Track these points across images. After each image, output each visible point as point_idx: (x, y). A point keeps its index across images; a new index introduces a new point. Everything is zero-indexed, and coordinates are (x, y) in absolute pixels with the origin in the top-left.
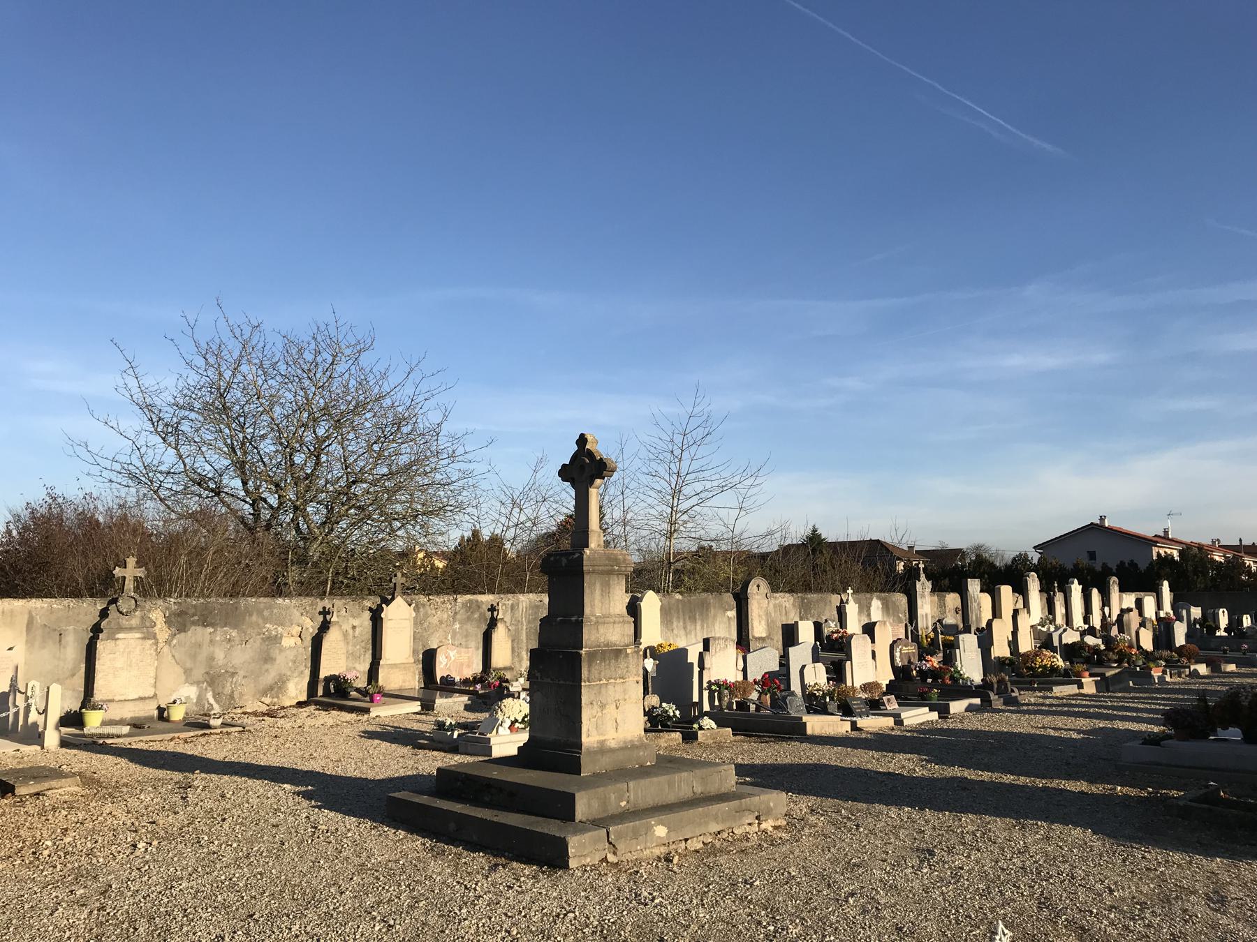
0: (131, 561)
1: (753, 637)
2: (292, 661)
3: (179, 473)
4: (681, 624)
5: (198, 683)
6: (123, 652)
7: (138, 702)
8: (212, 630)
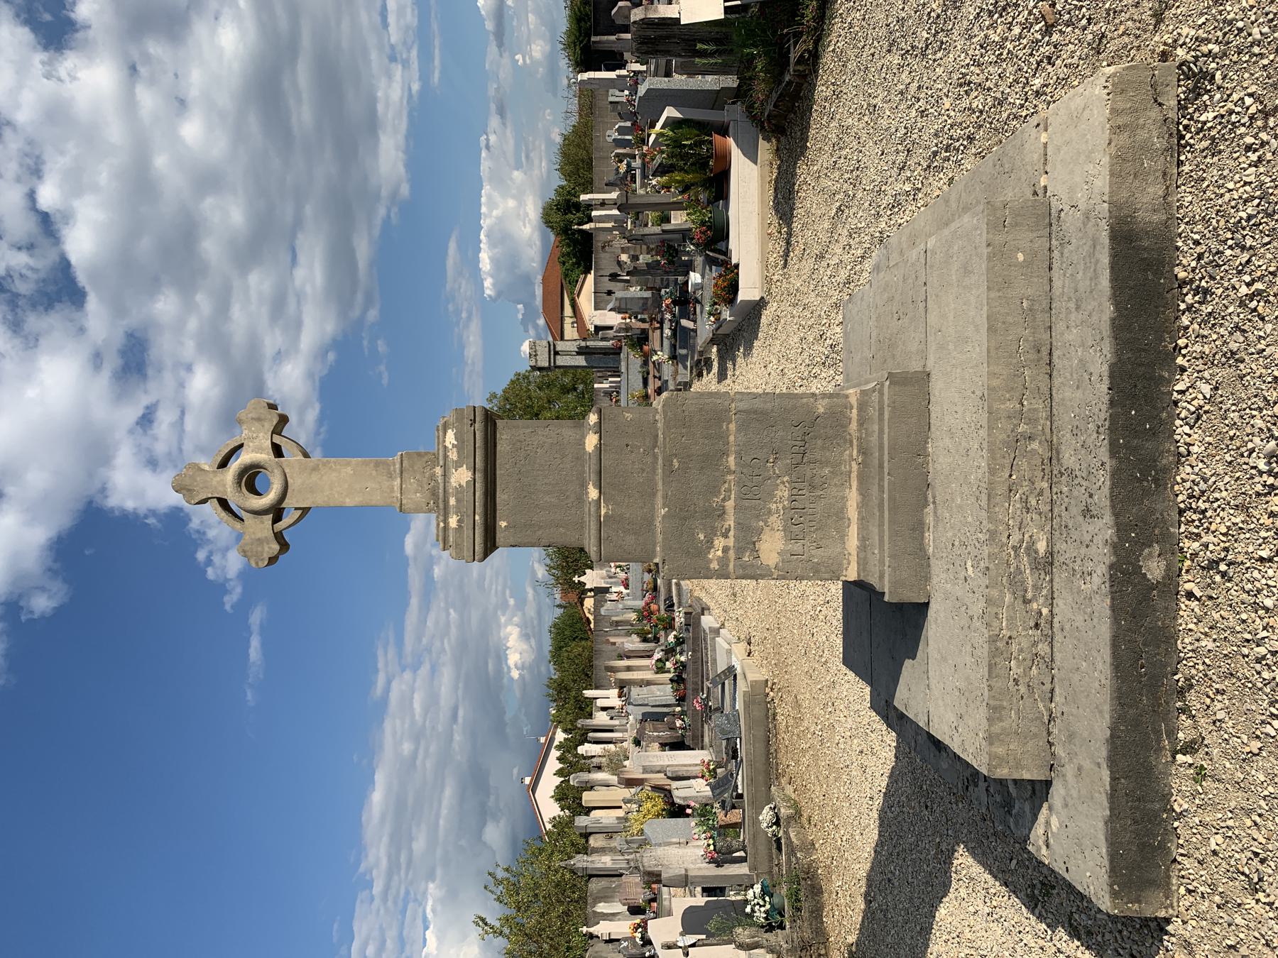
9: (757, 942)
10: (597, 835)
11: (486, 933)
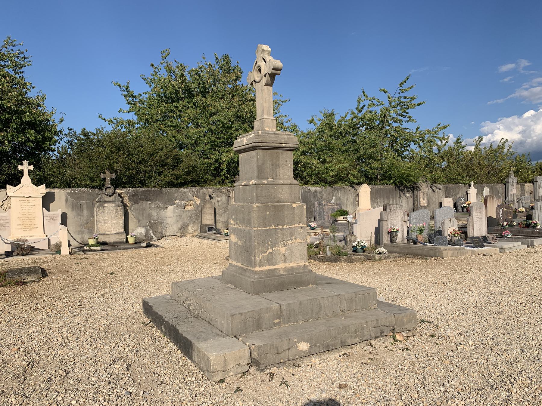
0: (20, 168)
1: (420, 206)
2: (189, 217)
3: (171, 126)
4: (382, 200)
5: (145, 227)
6: (108, 212)
7: (116, 235)
8: (150, 203)
9: (348, 242)
10: (533, 187)
11: (477, 142)
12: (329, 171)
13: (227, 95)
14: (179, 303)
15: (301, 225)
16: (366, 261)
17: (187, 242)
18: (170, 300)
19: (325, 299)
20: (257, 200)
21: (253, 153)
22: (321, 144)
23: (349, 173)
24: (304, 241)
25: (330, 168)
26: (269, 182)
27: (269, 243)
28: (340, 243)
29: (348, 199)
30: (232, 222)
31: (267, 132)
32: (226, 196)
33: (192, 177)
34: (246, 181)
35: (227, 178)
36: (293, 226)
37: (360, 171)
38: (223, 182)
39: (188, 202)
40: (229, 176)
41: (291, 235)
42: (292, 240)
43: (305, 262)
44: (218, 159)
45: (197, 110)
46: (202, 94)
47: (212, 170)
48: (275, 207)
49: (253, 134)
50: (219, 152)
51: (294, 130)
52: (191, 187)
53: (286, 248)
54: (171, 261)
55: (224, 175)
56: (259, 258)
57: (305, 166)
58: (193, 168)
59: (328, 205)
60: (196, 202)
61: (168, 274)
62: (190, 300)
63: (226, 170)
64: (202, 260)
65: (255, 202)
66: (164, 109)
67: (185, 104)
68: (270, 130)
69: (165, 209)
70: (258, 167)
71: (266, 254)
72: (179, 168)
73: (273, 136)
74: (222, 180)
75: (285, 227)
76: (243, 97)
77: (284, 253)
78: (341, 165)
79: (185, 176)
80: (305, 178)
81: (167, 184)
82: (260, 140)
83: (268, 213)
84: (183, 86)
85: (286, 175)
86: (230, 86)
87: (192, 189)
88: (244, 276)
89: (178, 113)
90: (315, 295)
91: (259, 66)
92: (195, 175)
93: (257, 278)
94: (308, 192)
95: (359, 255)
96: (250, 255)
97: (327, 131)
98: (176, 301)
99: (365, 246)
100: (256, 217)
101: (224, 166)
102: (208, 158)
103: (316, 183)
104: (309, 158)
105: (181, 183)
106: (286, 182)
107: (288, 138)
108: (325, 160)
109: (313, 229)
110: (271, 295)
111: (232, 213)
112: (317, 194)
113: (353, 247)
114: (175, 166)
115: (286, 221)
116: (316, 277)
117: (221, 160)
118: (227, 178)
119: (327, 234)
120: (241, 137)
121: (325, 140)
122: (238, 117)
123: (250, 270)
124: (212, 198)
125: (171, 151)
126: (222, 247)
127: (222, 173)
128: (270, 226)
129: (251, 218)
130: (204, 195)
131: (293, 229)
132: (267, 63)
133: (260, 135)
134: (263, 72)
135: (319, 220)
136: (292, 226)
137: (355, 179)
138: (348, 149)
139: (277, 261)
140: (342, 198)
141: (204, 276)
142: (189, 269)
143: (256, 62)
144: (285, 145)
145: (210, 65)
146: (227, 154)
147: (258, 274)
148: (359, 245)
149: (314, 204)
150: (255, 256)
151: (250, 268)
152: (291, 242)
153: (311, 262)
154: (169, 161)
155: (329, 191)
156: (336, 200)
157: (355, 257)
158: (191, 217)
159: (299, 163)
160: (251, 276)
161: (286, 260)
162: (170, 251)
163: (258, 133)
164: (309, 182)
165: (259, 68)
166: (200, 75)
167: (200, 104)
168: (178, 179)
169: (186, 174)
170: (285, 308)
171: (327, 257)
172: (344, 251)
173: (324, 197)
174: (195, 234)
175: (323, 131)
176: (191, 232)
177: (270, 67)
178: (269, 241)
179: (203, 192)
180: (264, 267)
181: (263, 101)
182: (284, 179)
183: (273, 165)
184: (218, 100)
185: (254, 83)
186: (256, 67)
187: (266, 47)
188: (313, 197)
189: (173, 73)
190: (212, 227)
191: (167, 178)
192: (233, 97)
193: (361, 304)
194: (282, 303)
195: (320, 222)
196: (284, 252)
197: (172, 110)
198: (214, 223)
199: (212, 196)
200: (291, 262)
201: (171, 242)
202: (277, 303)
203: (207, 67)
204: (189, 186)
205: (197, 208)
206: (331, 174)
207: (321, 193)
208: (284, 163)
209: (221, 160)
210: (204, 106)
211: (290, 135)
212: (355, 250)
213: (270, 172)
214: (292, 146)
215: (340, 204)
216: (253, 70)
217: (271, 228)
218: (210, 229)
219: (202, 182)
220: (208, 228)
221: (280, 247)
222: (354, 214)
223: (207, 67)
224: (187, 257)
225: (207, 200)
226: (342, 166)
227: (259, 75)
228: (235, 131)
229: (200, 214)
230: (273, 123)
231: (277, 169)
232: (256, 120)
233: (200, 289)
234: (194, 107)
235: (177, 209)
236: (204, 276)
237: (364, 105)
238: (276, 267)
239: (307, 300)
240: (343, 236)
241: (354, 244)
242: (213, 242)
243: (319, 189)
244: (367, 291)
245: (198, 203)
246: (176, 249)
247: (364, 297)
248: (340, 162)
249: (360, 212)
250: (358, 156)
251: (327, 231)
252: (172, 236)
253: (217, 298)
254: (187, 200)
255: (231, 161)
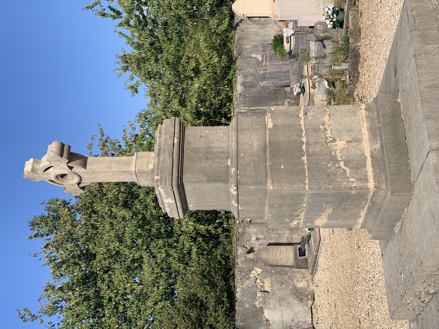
2: (281, 285)
12: (212, 63)
13: (92, 221)
14: (424, 310)
15: (301, 115)
16: (357, 7)
17: (322, 290)
18: (417, 322)
19: (421, 79)
20: (261, 183)
21: (188, 188)
22: (169, 76)
23: (215, 31)
24: (328, 110)
25: (206, 62)
26: (234, 164)
27: (330, 165)
28: (326, 47)
29: (256, 34)
30: (295, 222)
31: (156, 166)
32: (249, 227)
33: (218, 278)
34: (232, 200)
35: (221, 224)
36: (303, 127)
37: (212, 14)
38: (226, 230)
39: (259, 287)
40: (217, 221)
41: (316, 130)
42: (325, 129)
43: (361, 109)
44: (192, 237)
45: (114, 269)
46: (90, 260)
47: (208, 246)
48: (273, 156)
49: (159, 188)
50: (181, 235)
51: (146, 118)
52: (234, 281)
53: (337, 139)
54: (354, 317)
55: (216, 228)
56: (354, 182)
57: (202, 101)
58: (204, 276)
59: (266, 65)
60: (258, 274)
61: (374, 322)
62: (420, 292)
63: (208, 225)
64: (353, 267)
65: (264, 187)
66: (114, 319)
67: (104, 287)
68: (153, 161)
69: (269, 324)
70: (209, 181)
71: (348, 171)
72: (204, 299)
73: (162, 157)
74: (223, 232)
75: (304, 140)
76: (95, 196)
77: (347, 142)
78: (203, 45)
79: (218, 290)
80: (221, 100)
81: (230, 318)
82: (169, 177)
83: (282, 167)
84: (77, 289)
85: (223, 137)
86: (78, 217)
87: (238, 279)
88: (382, 206)
89: (119, 298)
90: (415, 94)
91: (57, 177)
92: (215, 274)
93: (387, 186)
94: (245, 97)
95: (348, 18)
96: (348, 196)
97: (151, 66)
98: (420, 314)
99: (333, 9)
100: (288, 186)
101: (202, 228)
102: (189, 253)
103: (230, 83)
104: (191, 93)
105: (228, 297)
106: (233, 137)
107: (165, 134)
108: (193, 70)
109: (303, 89)
110: (415, 164)
111: (280, 223)
112: (248, 82)
113: (334, 27)
114: (202, 305)
115: (295, 138)
116: (385, 92)
117: (193, 233)
118: (221, 224)
119: (313, 68)
120: (163, 207)
121: (161, 68)
122: (126, 205)
123: (373, 196)
124: (252, 248)
125: (179, 311)
126: (331, 236)
127: (213, 232)
128: (302, 163)
129: (290, 194)
130: (247, 260)
131: (308, 127)
132: (52, 165)
133: (161, 177)
134: (66, 170)
135: (289, 79)
136: (303, 129)
137: (223, 22)
138: (177, 33)
139: (359, 153)
140: (254, 43)
141: (379, 266)
142: (367, 289)
143: (50, 181)
144: (175, 139)
145: (46, 247)
146: (184, 223)
147: (379, 183)
148: (332, 17)
149: (263, 87)
150: (351, 189)
151: (370, 197)
152: (329, 131)
153: (358, 95)
154: (193, 315)
155: (243, 63)
156: (257, 52)
157: (350, 24)
158: (282, 283)
159: (197, 111)
160: (383, 194)
161: (357, 138)
162: (336, 318)
163: (157, 180)
164: (228, 94)
165: (59, 176)
166: (61, 262)
167: (106, 263)
168: (222, 301)
169: (213, 288)
170: (436, 143)
171: (350, 69)
172: (341, 42)
173: (252, 71)
174: (309, 277)
175: (149, 72)
176: (306, 283)
177: (58, 161)
178: (326, 165)
179: (242, 262)
180: (368, 174)
181: (109, 172)
182: (229, 141)
183: (207, 158)
184: (100, 235)
185: (81, 185)
186: (58, 182)
187: (28, 166)
188: (252, 89)
189: (57, 303)
190: (298, 249)
191: (220, 319)
192: (95, 212)
193: (429, 21)
194: (427, 147)
195: (293, 78)
196: (344, 143)
197: (115, 307)
198: (292, 246)
199: (249, 248)
200: (361, 130)
201: (321, 315)
202: (427, 156)
203: (48, 251)
204: (233, 285)
205: (267, 272)
206: (216, 59)
207: (245, 77)
208: (203, 140)
209: (193, 233)
210: (109, 257)
211: (160, 130)
212: (339, 24)
213: (217, 162)
214: (177, 127)
215: (264, 46)
216: (62, 186)
217: (306, 162)
218: (302, 253)
219: (226, 263)
220: (300, 256)
221: (337, 148)
222: (281, 24)
223: (48, 251)
224: (346, 292)
225: (255, 256)
226: (204, 43)
227: (69, 177)
228: (147, 211)
229: (277, 267)
230: (141, 157)
231: (212, 152)
232: (137, 182)
233: (403, 275)
234: (110, 273)
235: (270, 304)
236: (379, 266)
237: (110, 7)
238: (368, 154)
239: (423, 107)
240: (317, 43)
241: (330, 26)
242: (323, 249)
243: (239, 79)
244: (409, 12)
245: (259, 271)
246: (334, 309)
247: (419, 16)
248: (197, 45)
249: (278, 13)
250: (189, 18)
251: (307, 70)
252: (312, 314)
253: (417, 250)
254: (255, 289)
255: (194, 218)
